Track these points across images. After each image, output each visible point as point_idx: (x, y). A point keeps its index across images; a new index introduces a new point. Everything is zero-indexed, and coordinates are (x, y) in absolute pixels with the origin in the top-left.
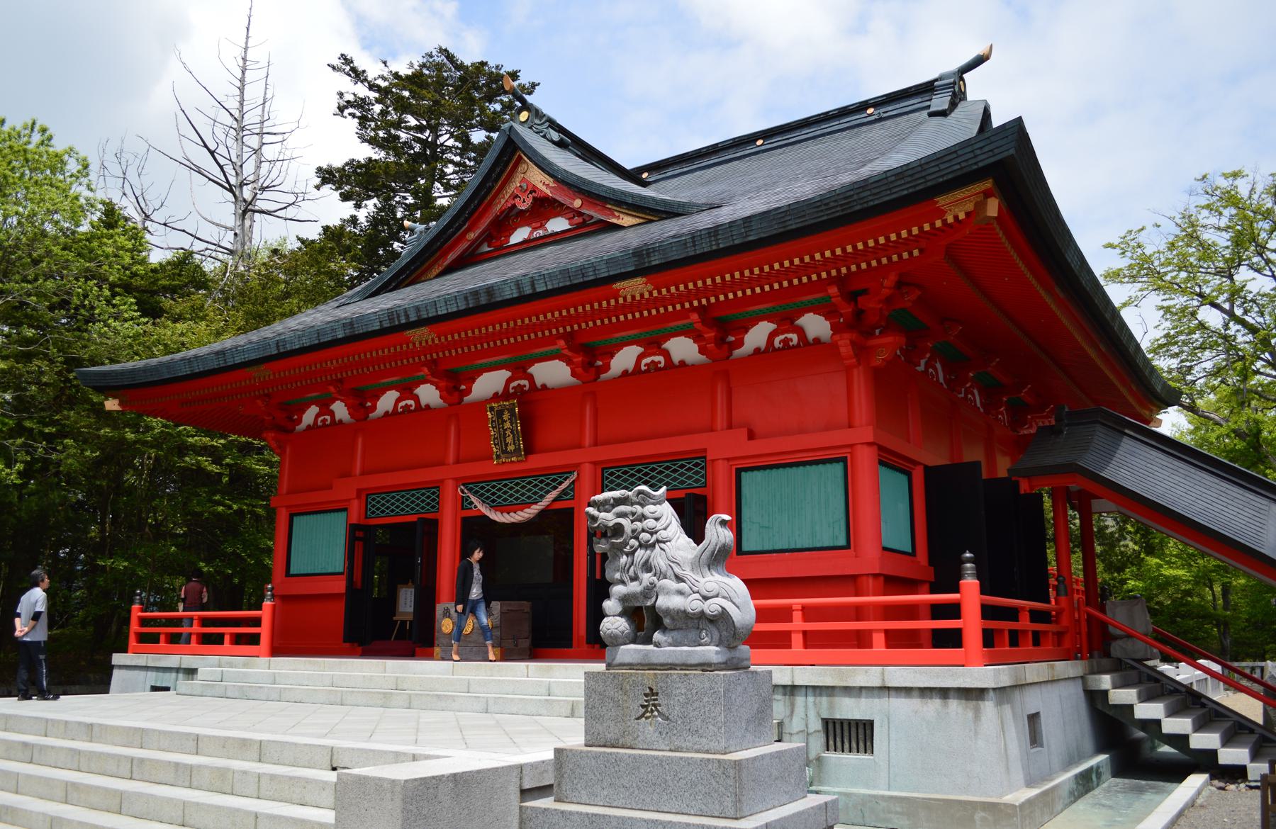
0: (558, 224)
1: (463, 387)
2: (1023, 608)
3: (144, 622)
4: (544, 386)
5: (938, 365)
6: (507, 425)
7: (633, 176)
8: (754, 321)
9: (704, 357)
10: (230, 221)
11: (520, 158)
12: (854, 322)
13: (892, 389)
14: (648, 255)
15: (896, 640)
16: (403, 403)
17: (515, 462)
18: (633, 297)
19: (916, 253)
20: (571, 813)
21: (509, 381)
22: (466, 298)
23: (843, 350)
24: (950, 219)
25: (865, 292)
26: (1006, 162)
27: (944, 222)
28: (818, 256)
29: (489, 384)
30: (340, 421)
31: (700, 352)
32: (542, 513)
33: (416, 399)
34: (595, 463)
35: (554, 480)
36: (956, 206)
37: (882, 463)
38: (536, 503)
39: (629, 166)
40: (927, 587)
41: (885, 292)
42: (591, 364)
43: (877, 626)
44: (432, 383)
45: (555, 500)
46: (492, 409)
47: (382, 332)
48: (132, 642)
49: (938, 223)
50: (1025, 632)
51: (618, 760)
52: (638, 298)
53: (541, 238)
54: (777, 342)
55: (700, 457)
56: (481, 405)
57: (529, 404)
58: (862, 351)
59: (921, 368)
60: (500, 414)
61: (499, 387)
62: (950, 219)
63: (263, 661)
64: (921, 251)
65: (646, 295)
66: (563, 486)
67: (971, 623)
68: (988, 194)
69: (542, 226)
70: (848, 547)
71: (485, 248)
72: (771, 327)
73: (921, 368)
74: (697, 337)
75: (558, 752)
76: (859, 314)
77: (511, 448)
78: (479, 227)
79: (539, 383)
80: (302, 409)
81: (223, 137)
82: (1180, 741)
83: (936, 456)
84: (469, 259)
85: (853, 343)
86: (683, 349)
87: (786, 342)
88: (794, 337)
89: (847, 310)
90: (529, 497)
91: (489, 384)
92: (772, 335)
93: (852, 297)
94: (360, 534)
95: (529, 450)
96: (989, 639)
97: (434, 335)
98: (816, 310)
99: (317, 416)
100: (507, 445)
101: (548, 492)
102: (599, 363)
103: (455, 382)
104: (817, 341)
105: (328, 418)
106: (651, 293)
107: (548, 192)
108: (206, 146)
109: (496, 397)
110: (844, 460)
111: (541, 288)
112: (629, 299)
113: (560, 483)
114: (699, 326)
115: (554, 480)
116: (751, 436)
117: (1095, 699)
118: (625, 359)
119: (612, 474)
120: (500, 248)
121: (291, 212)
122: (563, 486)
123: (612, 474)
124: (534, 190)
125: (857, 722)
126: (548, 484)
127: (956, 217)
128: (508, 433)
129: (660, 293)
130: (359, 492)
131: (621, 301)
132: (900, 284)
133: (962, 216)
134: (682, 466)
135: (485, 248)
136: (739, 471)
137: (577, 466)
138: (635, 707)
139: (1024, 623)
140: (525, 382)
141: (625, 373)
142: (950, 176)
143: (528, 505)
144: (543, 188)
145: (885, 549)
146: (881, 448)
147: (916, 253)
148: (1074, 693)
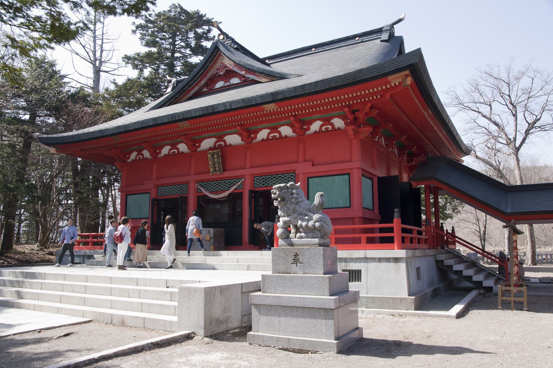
0: (235, 81)
1: (197, 145)
2: (415, 229)
4: (230, 145)
5: (383, 139)
6: (216, 160)
7: (262, 61)
8: (315, 120)
9: (294, 134)
10: (92, 75)
11: (220, 54)
12: (353, 120)
13: (367, 147)
14: (277, 95)
15: (371, 241)
16: (172, 151)
17: (218, 175)
18: (270, 111)
19: (379, 96)
20: (269, 296)
21: (216, 142)
22: (203, 110)
23: (349, 132)
25: (358, 110)
26: (415, 66)
27: (391, 86)
28: (342, 97)
29: (207, 143)
30: (146, 158)
32: (230, 194)
33: (178, 149)
35: (235, 181)
36: (395, 80)
37: (363, 176)
38: (227, 190)
39: (261, 56)
40: (378, 222)
41: (366, 110)
42: (249, 136)
43: (364, 237)
44: (184, 143)
45: (235, 189)
46: (210, 153)
47: (168, 123)
49: (388, 86)
50: (415, 238)
51: (285, 278)
52: (272, 111)
56: (205, 152)
57: (224, 151)
58: (356, 133)
59: (377, 140)
60: (213, 155)
61: (265, 137)
62: (393, 85)
64: (381, 96)
65: (275, 110)
66: (238, 184)
67: (397, 234)
68: (407, 76)
69: (228, 81)
70: (350, 207)
71: (205, 89)
73: (377, 140)
74: (292, 126)
75: (263, 276)
76: (356, 119)
77: (217, 169)
78: (200, 81)
79: (228, 143)
80: (130, 153)
81: (88, 41)
82: (469, 278)
83: (381, 173)
84: (198, 95)
85: (353, 129)
86: (286, 131)
87: (327, 129)
88: (330, 127)
89: (351, 117)
90: (224, 188)
91: (207, 143)
92: (322, 126)
93: (353, 112)
94: (156, 202)
95: (224, 170)
96: (403, 240)
97: (189, 124)
98: (339, 117)
99: (137, 156)
101: (232, 186)
102: (253, 136)
103: (194, 143)
104: (339, 129)
105: (141, 156)
106: (277, 110)
107: (231, 68)
108: (81, 44)
109: (211, 149)
110: (349, 174)
111: (234, 107)
112: (268, 112)
113: (237, 183)
114: (294, 122)
115: (235, 181)
116: (313, 165)
117: (439, 263)
118: (263, 134)
119: (258, 179)
120: (211, 90)
121: (116, 72)
122: (238, 184)
123: (258, 179)
124: (226, 67)
125: (355, 271)
126: (232, 183)
127: (395, 84)
129: (281, 109)
130: (155, 185)
131: (265, 112)
132: (371, 108)
133: (397, 84)
135: (205, 89)
136: (308, 178)
137: (243, 176)
138: (291, 259)
139: (415, 235)
140: (223, 143)
141: (263, 140)
142: (394, 69)
143: (225, 191)
144: (230, 66)
145: (364, 208)
146: (363, 170)
147: (379, 96)
148: (431, 260)
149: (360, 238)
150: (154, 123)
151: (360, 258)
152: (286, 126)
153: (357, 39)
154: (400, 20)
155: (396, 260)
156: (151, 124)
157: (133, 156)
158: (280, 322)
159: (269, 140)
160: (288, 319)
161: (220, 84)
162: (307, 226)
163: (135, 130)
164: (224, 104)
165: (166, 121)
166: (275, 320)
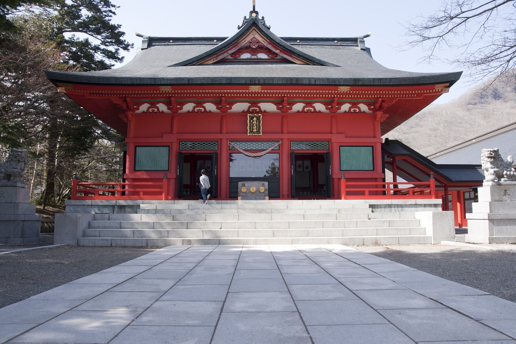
3: (347, 187)
22: (287, 80)
24: (437, 91)
34: (288, 139)
43: (367, 191)
53: (255, 59)
54: (150, 110)
55: (329, 141)
60: (252, 118)
61: (300, 109)
62: (437, 91)
63: (164, 201)
72: (149, 105)
86: (320, 107)
88: (156, 110)
92: (149, 108)
98: (163, 103)
100: (253, 129)
110: (169, 146)
119: (183, 143)
120: (236, 59)
134: (204, 143)
138: (502, 193)
149: (364, 191)
150: (228, 82)
152: (270, 104)
154: (368, 36)
155: (436, 206)
156: (224, 82)
157: (144, 107)
158: (507, 229)
159: (305, 112)
160: (512, 226)
161: (246, 56)
162: (510, 174)
163: (133, 85)
164: (309, 79)
165: (244, 82)
166: (504, 228)
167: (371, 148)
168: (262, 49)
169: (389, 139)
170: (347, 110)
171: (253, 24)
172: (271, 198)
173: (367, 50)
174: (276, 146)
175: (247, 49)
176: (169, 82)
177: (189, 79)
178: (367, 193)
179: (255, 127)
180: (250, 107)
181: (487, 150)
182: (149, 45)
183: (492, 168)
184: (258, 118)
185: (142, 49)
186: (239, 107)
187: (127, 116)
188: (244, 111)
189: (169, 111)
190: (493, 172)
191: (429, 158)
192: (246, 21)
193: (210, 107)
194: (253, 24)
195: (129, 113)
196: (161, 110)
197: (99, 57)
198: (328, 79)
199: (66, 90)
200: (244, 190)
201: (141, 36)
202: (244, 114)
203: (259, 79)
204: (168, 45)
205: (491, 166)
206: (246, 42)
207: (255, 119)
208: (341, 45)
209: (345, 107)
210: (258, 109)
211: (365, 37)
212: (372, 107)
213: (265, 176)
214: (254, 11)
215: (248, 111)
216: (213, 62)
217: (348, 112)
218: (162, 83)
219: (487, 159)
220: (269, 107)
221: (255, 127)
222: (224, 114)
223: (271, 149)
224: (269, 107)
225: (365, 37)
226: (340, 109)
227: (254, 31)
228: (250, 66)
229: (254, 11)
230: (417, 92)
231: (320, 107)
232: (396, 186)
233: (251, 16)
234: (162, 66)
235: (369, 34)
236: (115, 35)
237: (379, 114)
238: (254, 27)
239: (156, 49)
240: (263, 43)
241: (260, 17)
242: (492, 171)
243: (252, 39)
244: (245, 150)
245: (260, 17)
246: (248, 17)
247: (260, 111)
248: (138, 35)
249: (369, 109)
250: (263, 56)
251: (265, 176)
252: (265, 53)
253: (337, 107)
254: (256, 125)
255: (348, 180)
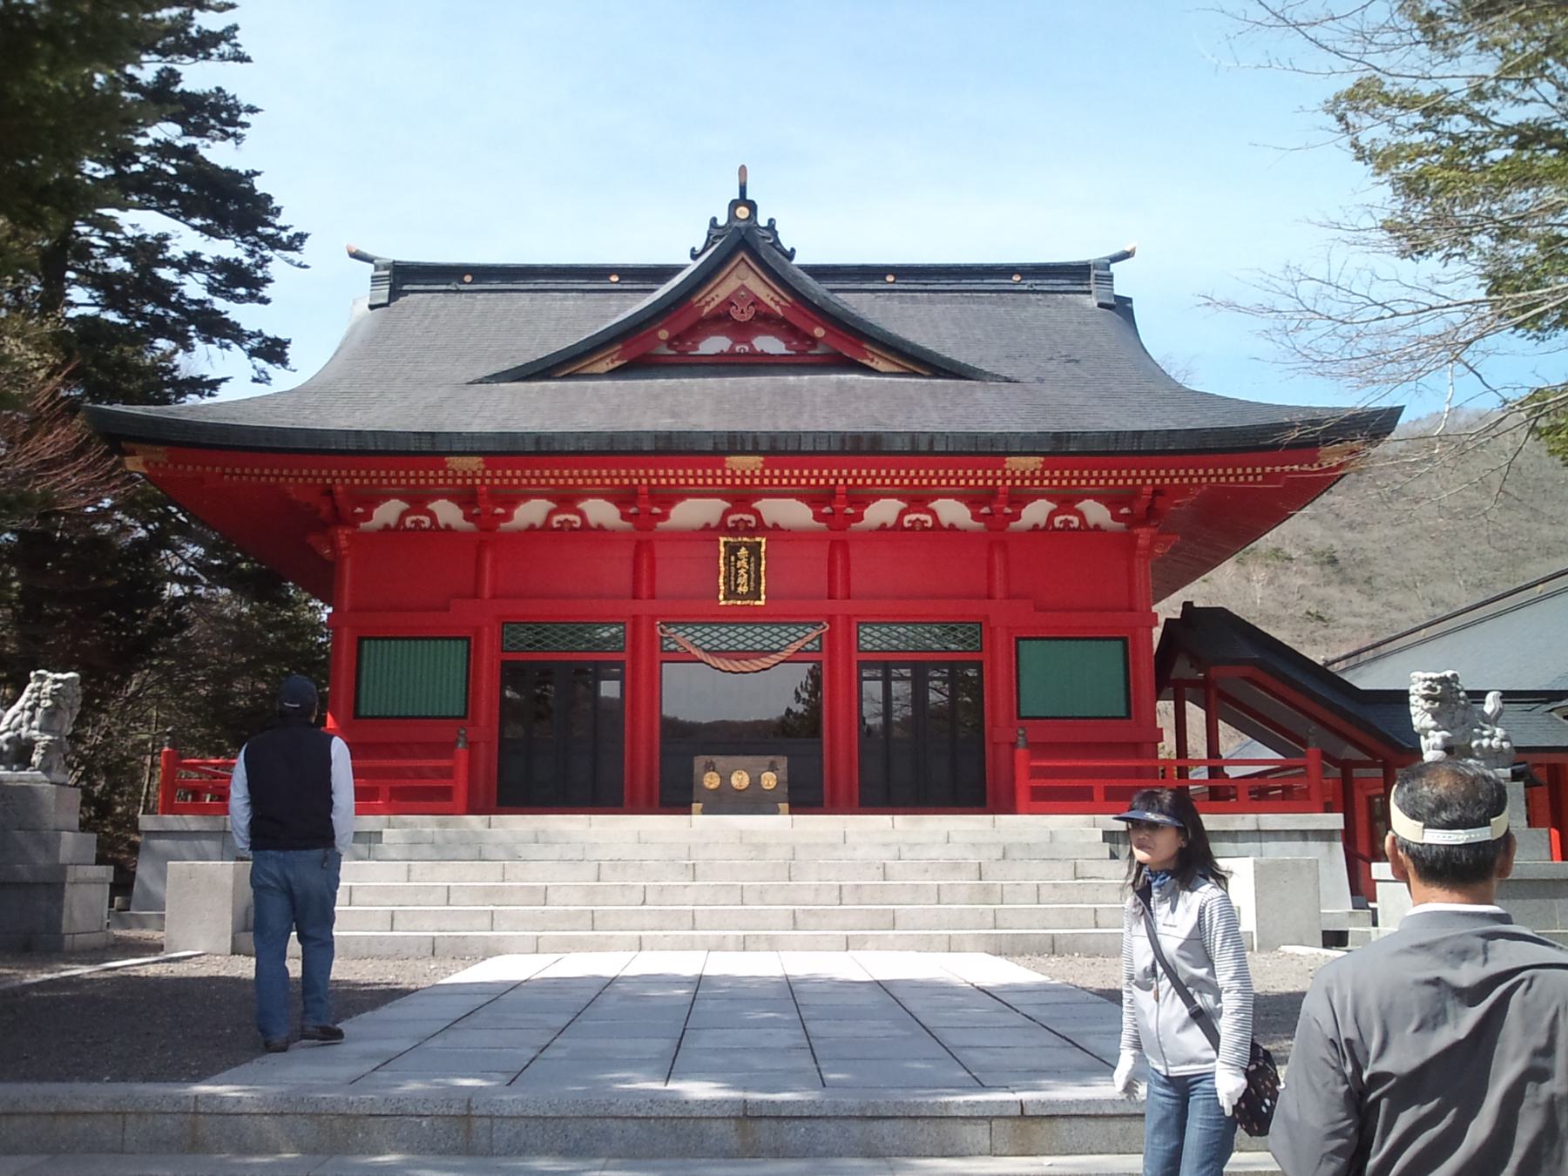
31: (1113, 518)
43: (1099, 785)
48: (1022, 795)
53: (746, 354)
54: (409, 521)
60: (732, 550)
61: (714, 519)
72: (404, 506)
86: (953, 512)
87: (1067, 522)
88: (1075, 521)
92: (404, 514)
100: (737, 586)
107: (778, 309)
120: (683, 354)
128: (742, 571)
136: (361, 640)
149: (1091, 788)
151: (1287, 831)
153: (1017, 278)
154: (1126, 255)
155: (1325, 835)
157: (388, 512)
161: (714, 345)
164: (913, 436)
165: (709, 446)
167: (1119, 644)
168: (765, 320)
169: (1196, 605)
170: (1042, 521)
171: (742, 239)
172: (794, 810)
173: (1122, 308)
174: (809, 638)
175: (720, 320)
176: (477, 446)
177: (538, 438)
178: (1098, 795)
179: (742, 580)
180: (726, 513)
181: (1423, 675)
182: (395, 294)
183: (1436, 729)
184: (754, 550)
185: (372, 307)
186: (692, 513)
187: (332, 542)
188: (707, 527)
189: (469, 526)
190: (1439, 741)
191: (1334, 668)
192: (715, 232)
193: (600, 511)
194: (742, 239)
195: (343, 535)
196: (441, 521)
197: (194, 287)
198: (974, 437)
199: (146, 463)
200: (711, 781)
201: (369, 260)
202: (708, 533)
203: (755, 437)
204: (458, 291)
205: (1433, 723)
206: (718, 301)
207: (743, 552)
208: (1035, 292)
209: (1036, 513)
210: (752, 518)
211: (1115, 259)
212: (1125, 511)
213: (789, 711)
214: (743, 200)
215: (723, 528)
216: (611, 366)
217: (1045, 528)
218: (458, 447)
219: (1422, 702)
220: (792, 513)
221: (742, 580)
222: (645, 540)
223: (794, 647)
224: (792, 513)
225: (1115, 259)
226: (1017, 517)
227: (743, 266)
228: (729, 382)
229: (743, 200)
230: (1257, 471)
231: (953, 512)
232: (1215, 772)
233: (732, 216)
234: (454, 390)
235: (1128, 249)
236: (233, 204)
237: (1144, 535)
238: (743, 255)
239: (416, 301)
240: (772, 304)
241: (762, 221)
242: (1437, 738)
243: (735, 292)
244: (705, 651)
245: (762, 221)
246: (722, 221)
247: (761, 528)
248: (356, 255)
249: (1115, 517)
250: (770, 344)
251: (789, 711)
252: (773, 334)
253: (1008, 510)
254: (748, 572)
255: (1037, 748)
